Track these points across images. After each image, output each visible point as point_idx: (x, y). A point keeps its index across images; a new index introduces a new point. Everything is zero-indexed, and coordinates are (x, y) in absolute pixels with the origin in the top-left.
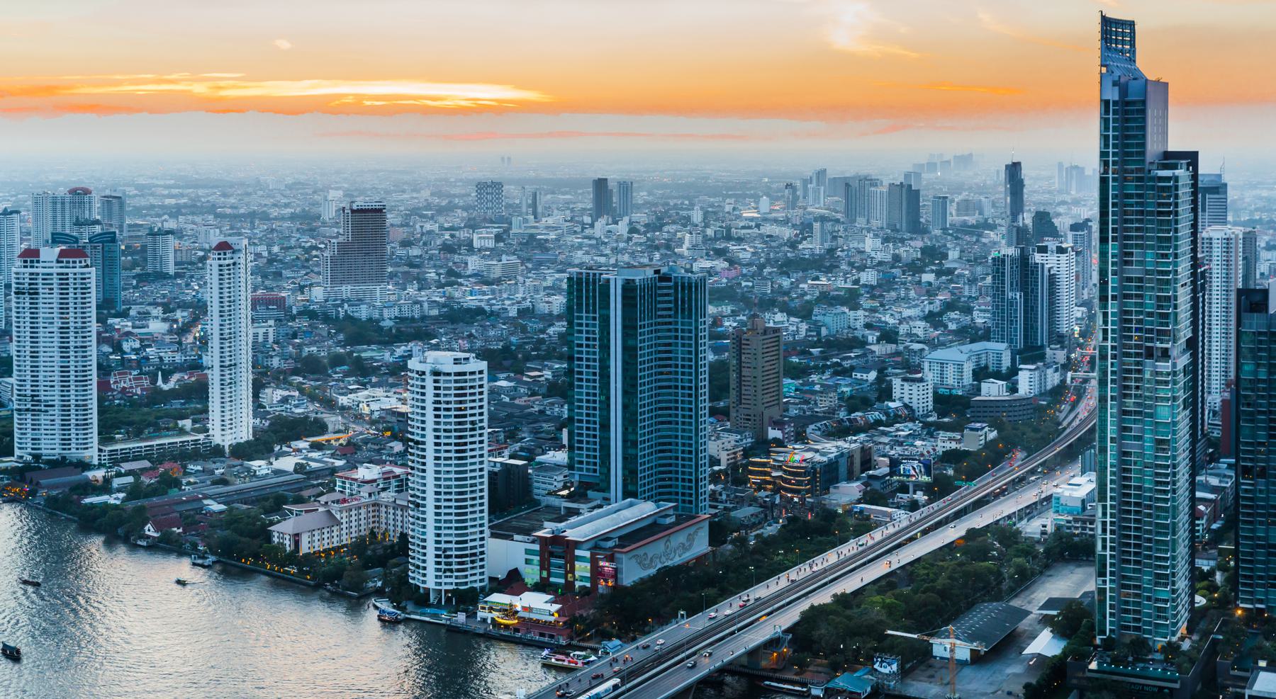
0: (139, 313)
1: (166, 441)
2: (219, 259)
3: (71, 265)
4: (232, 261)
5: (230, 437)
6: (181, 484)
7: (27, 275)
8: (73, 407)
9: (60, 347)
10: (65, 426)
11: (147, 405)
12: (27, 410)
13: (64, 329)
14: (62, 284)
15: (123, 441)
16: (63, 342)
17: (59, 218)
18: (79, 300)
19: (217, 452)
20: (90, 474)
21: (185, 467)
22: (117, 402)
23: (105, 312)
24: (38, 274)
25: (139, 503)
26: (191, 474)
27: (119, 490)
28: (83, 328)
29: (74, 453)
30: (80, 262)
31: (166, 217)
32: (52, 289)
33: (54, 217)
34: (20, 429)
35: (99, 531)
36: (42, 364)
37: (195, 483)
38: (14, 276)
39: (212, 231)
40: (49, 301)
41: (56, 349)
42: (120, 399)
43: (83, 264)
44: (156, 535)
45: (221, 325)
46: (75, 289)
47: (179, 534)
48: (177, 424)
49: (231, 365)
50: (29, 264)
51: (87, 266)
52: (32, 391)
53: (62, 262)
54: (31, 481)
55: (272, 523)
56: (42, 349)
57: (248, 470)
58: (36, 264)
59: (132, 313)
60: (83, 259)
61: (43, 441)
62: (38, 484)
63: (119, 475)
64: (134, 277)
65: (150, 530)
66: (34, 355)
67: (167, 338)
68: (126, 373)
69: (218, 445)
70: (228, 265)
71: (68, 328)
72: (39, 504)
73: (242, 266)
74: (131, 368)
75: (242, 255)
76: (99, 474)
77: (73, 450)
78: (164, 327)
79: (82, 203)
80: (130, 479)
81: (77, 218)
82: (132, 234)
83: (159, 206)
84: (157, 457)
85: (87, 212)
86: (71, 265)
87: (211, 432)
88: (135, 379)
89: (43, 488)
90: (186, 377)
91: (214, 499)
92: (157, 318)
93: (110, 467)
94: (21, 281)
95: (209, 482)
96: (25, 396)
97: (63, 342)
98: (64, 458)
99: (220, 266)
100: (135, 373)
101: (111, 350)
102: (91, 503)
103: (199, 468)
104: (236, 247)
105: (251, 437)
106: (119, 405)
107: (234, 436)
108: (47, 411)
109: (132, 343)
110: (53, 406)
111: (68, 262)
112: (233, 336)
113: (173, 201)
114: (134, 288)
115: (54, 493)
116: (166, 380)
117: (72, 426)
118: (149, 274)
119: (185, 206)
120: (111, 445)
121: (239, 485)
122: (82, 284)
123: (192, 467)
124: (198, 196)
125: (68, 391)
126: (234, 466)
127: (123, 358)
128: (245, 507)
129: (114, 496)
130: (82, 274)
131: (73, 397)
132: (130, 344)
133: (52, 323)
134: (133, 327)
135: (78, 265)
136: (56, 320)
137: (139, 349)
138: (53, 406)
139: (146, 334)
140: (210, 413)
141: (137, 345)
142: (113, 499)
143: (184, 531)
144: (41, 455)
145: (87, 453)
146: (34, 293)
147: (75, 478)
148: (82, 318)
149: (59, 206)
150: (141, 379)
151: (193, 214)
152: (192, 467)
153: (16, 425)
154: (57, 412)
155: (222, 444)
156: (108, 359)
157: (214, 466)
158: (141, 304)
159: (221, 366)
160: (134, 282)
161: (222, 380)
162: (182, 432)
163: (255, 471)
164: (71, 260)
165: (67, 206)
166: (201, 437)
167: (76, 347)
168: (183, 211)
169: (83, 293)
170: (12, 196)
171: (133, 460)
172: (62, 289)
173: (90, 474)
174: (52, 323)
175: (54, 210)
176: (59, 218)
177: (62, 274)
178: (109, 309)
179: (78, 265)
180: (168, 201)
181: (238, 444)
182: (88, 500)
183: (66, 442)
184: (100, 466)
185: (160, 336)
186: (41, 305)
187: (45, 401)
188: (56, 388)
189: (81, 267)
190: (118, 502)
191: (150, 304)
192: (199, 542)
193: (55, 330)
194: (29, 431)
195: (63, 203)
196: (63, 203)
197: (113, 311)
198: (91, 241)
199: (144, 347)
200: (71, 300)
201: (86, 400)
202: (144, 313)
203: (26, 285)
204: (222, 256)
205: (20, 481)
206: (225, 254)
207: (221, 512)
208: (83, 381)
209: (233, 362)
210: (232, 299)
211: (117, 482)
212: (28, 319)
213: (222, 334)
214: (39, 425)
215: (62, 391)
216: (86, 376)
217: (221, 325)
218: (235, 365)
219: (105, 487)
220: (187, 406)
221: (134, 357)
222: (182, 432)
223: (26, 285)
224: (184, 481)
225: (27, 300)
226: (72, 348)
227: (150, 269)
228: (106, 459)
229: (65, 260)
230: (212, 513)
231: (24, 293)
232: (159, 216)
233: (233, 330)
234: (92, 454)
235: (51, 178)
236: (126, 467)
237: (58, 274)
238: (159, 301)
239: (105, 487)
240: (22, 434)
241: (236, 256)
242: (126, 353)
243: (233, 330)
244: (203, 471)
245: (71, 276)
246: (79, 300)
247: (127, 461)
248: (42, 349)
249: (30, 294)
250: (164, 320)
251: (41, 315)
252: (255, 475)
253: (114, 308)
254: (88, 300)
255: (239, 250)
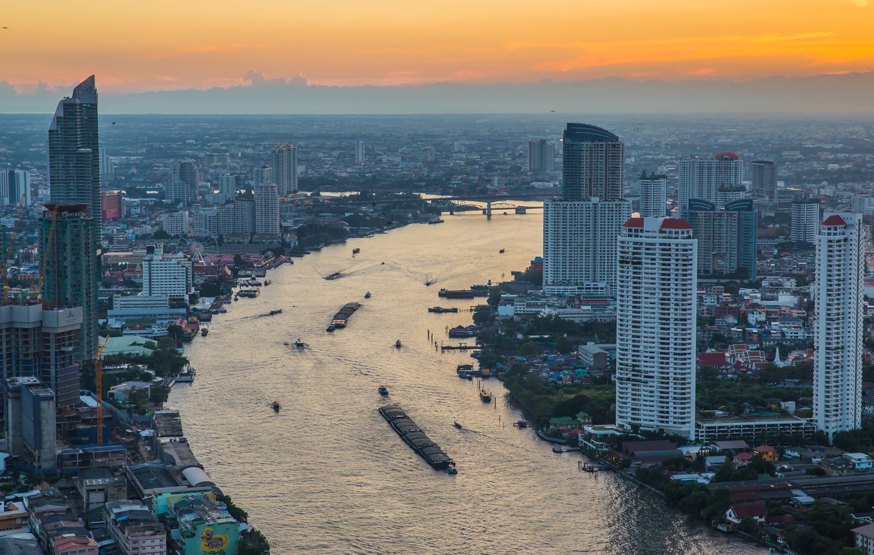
0: (771, 284)
1: (766, 423)
2: (829, 234)
3: (674, 235)
4: (842, 237)
5: (834, 424)
6: (774, 469)
7: (631, 244)
8: (671, 380)
9: (661, 319)
10: (664, 399)
11: (759, 382)
12: (628, 379)
13: (665, 301)
14: (664, 255)
15: (722, 418)
16: (664, 314)
17: (705, 183)
18: (681, 272)
19: (819, 439)
20: (685, 450)
21: (781, 453)
22: (730, 376)
23: (738, 281)
24: (641, 244)
25: (727, 486)
26: (787, 459)
27: (711, 470)
28: (683, 300)
29: (672, 427)
30: (683, 233)
31: (825, 183)
32: (654, 259)
33: (701, 184)
34: (622, 398)
35: (683, 511)
36: (643, 334)
37: (789, 470)
38: (619, 244)
39: (867, 200)
40: (651, 272)
41: (656, 320)
42: (734, 373)
43: (686, 235)
44: (736, 521)
45: (829, 305)
46: (677, 260)
47: (761, 523)
48: (780, 406)
49: (838, 348)
50: (633, 233)
51: (689, 237)
52: (634, 361)
53: (665, 232)
54: (627, 452)
55: (857, 525)
56: (643, 320)
57: (847, 461)
58: (640, 234)
59: (765, 284)
60: (685, 230)
61: (642, 412)
62: (633, 454)
63: (713, 453)
64: (776, 246)
65: (731, 516)
66: (636, 325)
67: (795, 314)
68: (743, 347)
69: (822, 432)
70: (839, 241)
71: (669, 300)
72: (631, 475)
73: (853, 242)
74: (751, 342)
75: (854, 231)
76: (694, 450)
77: (671, 424)
78: (794, 300)
79: (728, 168)
80: (722, 459)
81: (723, 184)
82: (783, 201)
83: (821, 172)
84: (755, 438)
85: (733, 178)
86: (674, 235)
87: (814, 417)
88: (751, 354)
89: (638, 460)
90: (805, 355)
91: (804, 490)
92: (788, 290)
93: (707, 445)
94: (626, 250)
95: (804, 471)
96: (627, 365)
97: (664, 314)
98: (662, 431)
99: (830, 241)
100: (755, 347)
101: (736, 322)
102: (679, 481)
103: (796, 454)
104: (848, 222)
105: (859, 426)
106: (732, 379)
107: (840, 423)
108: (646, 382)
109: (758, 316)
110: (652, 377)
111: (671, 233)
112: (841, 317)
113: (836, 166)
114: (775, 257)
115: (647, 465)
116: (783, 357)
117: (670, 399)
118: (792, 244)
119: (848, 171)
120: (710, 421)
121: (835, 476)
122: (684, 255)
123: (789, 452)
124: (864, 161)
125: (668, 363)
126: (834, 456)
127: (744, 331)
128: (835, 502)
129: (704, 475)
130: (684, 245)
131: (671, 370)
132: (755, 316)
133: (654, 294)
134: (762, 299)
135: (680, 235)
136: (657, 290)
137: (764, 322)
138: (652, 377)
139: (774, 307)
140: (814, 397)
141: (763, 318)
142: (703, 479)
143: (767, 521)
144: (640, 425)
145: (685, 428)
146: (637, 263)
147: (668, 452)
148: (683, 290)
149: (705, 171)
150: (757, 354)
151: (854, 180)
152: (790, 453)
153: (618, 394)
154: (655, 384)
155: (826, 430)
156: (730, 331)
157: (812, 454)
158: (777, 274)
159: (827, 349)
160: (776, 251)
161: (827, 363)
162: (785, 414)
163: (854, 464)
164: (674, 230)
165: (714, 171)
166: (804, 421)
167: (676, 320)
168: (845, 177)
169: (684, 265)
170: (677, 159)
171: (730, 439)
172: (664, 260)
173: (685, 450)
174: (654, 294)
175: (701, 175)
176: (705, 183)
177: (665, 244)
178: (742, 278)
179: (680, 235)
180: (831, 166)
181: (843, 433)
182: (676, 477)
183: (664, 414)
184: (697, 442)
185: (787, 310)
186: (644, 275)
187: (646, 372)
188: (656, 359)
189: (683, 238)
190: (706, 482)
191: (785, 275)
192: (779, 535)
193: (656, 300)
194: (629, 400)
195: (710, 168)
196: (710, 168)
197: (746, 281)
198: (727, 209)
199: (769, 320)
200: (672, 271)
201: (684, 374)
202: (777, 285)
203: (630, 254)
204: (832, 231)
205: (617, 450)
206: (836, 229)
207: (808, 505)
208: (682, 355)
209: (840, 345)
210: (842, 277)
211: (709, 461)
212: (630, 288)
213: (829, 315)
214: (639, 395)
215: (662, 363)
216: (685, 349)
217: (829, 305)
218: (843, 348)
219: (698, 465)
220: (800, 386)
221: (755, 331)
222: (785, 414)
223: (630, 254)
224: (778, 468)
225: (631, 269)
226: (672, 321)
227: (793, 238)
228: (703, 437)
229: (667, 230)
230: (801, 505)
231: (628, 263)
232: (818, 182)
233: (841, 311)
234: (689, 429)
235: (720, 141)
236: (720, 446)
237: (661, 244)
238: (795, 272)
239: (698, 465)
240: (623, 403)
241: (848, 231)
242: (750, 326)
243: (841, 311)
244: (801, 458)
245: (673, 246)
246: (681, 272)
247: (725, 440)
248: (643, 320)
249: (633, 263)
250: (795, 293)
251: (644, 285)
252: (854, 468)
253: (748, 278)
254: (689, 272)
255: (852, 226)
